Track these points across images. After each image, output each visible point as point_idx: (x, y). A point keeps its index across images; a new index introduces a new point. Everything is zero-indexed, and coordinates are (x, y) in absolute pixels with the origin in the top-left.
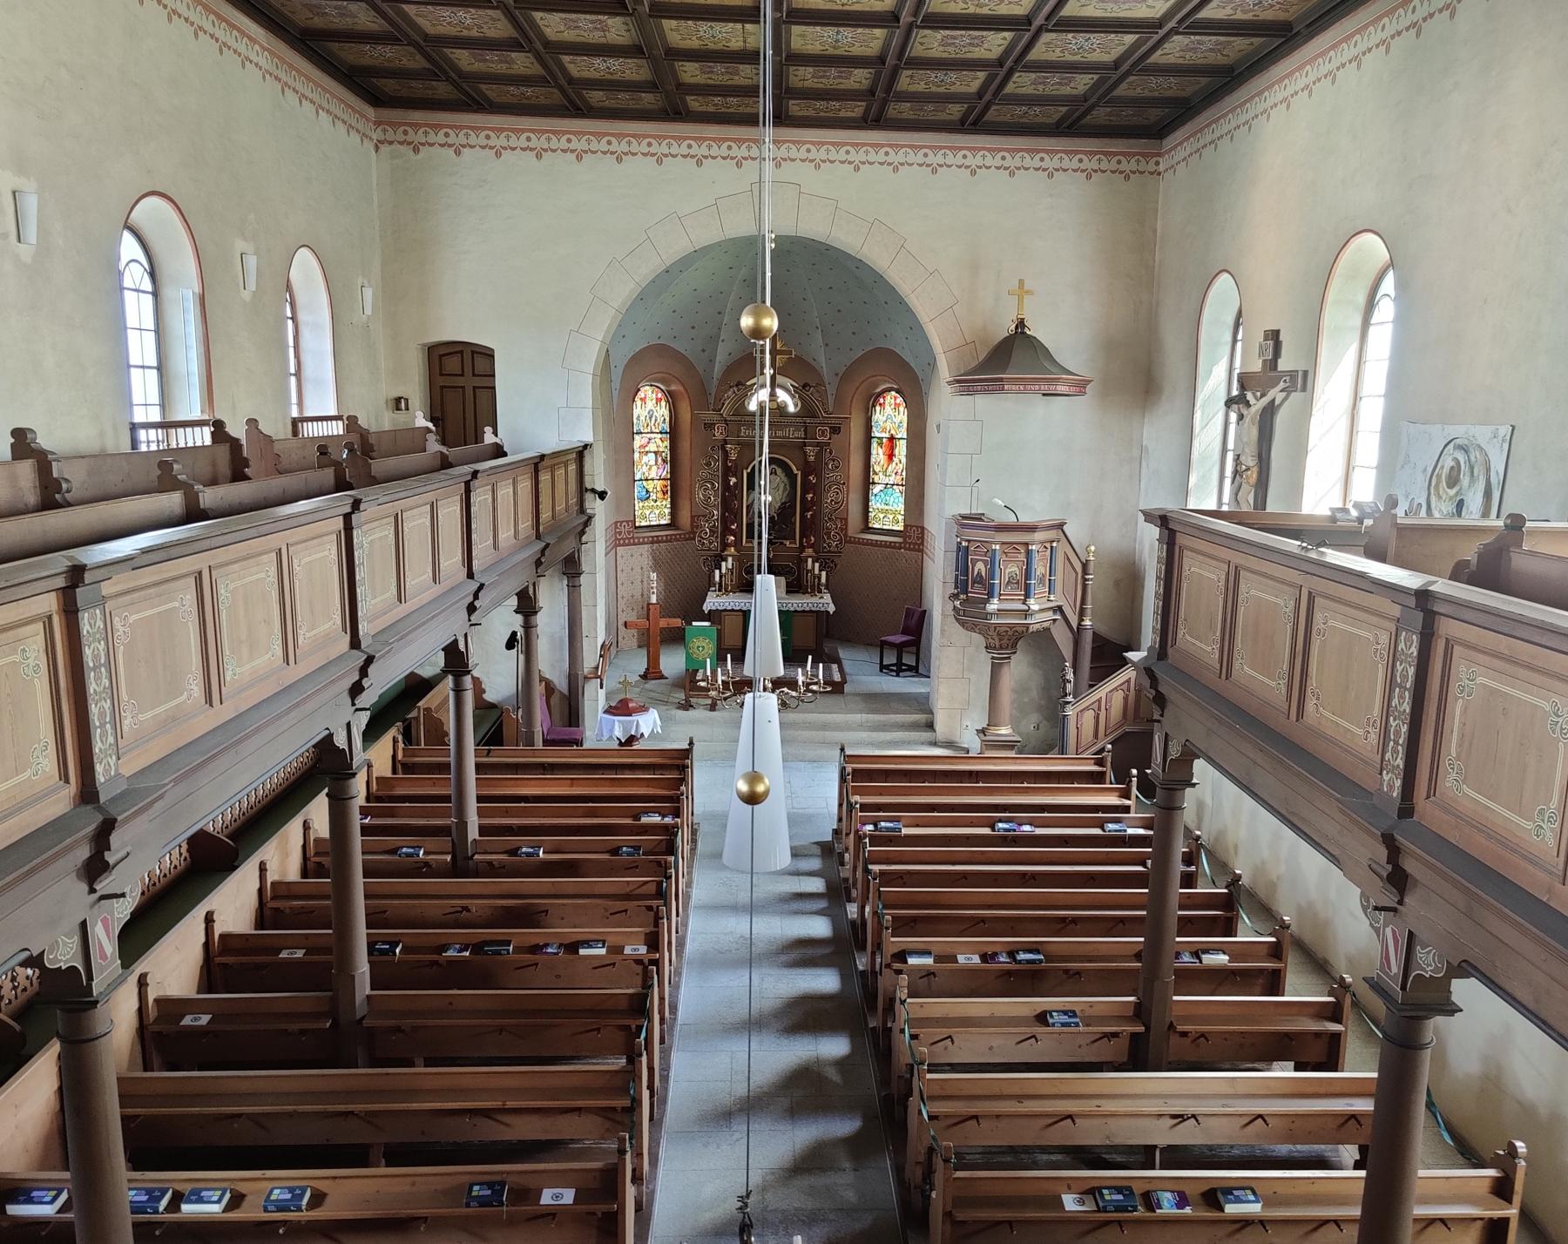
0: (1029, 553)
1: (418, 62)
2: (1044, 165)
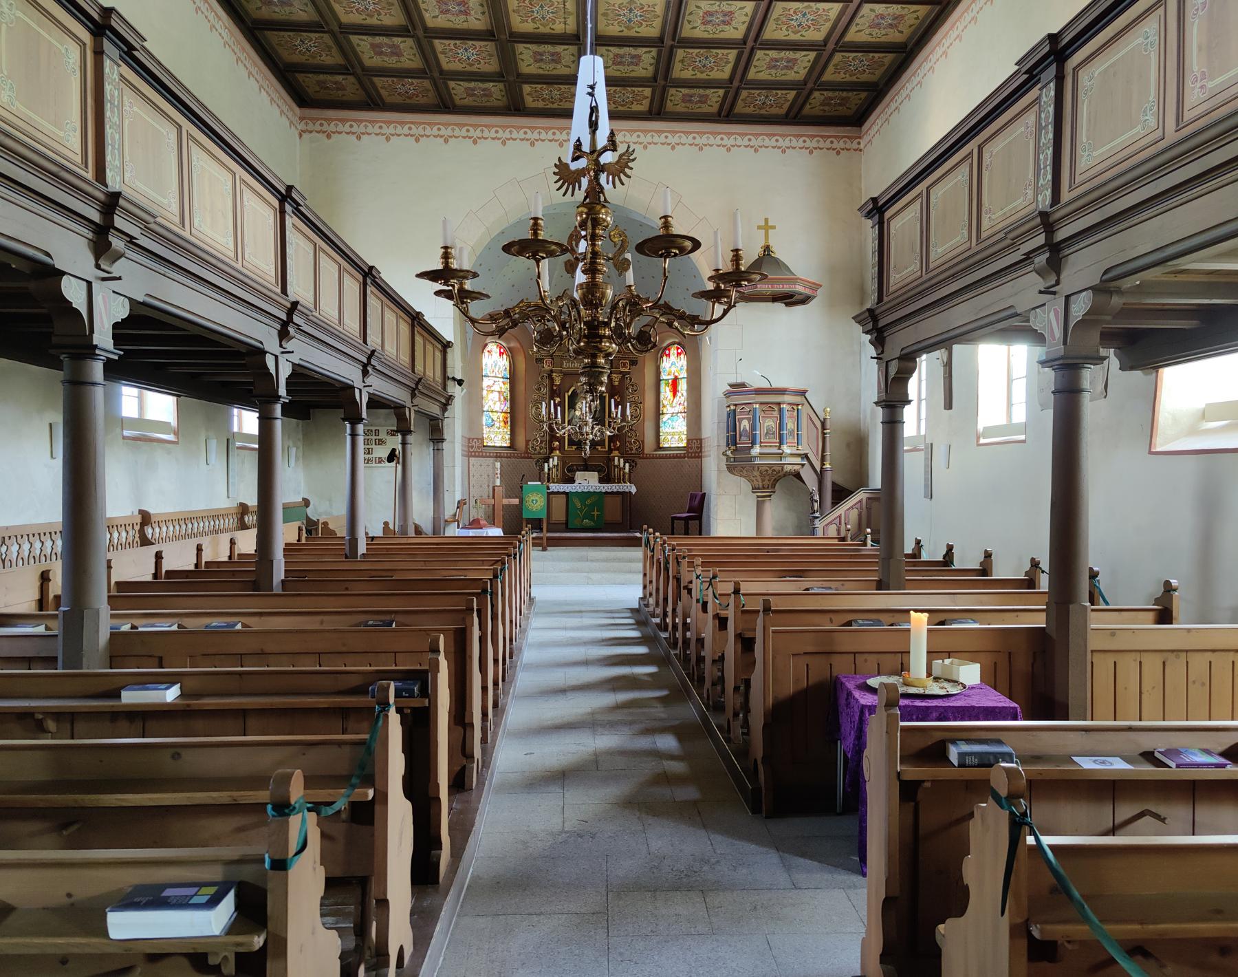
0: (780, 410)
1: (332, 58)
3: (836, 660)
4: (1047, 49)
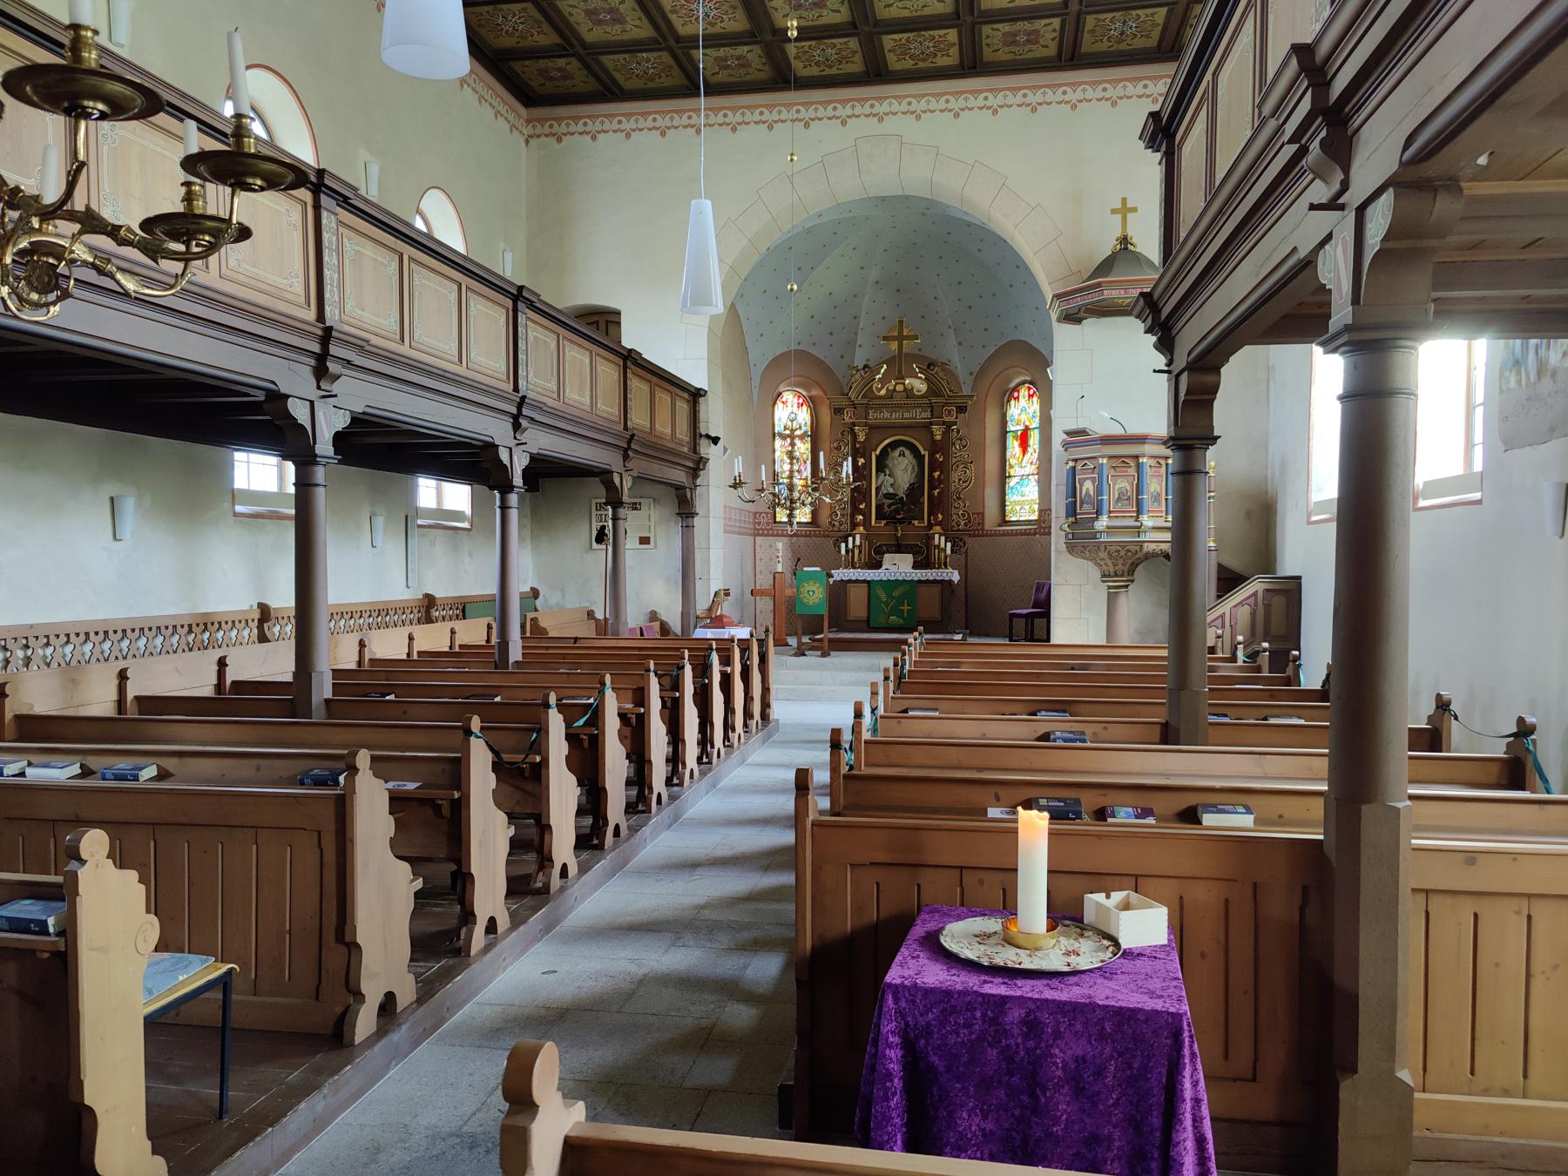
0: (1139, 466)
2: (1148, 91)
3: (927, 878)
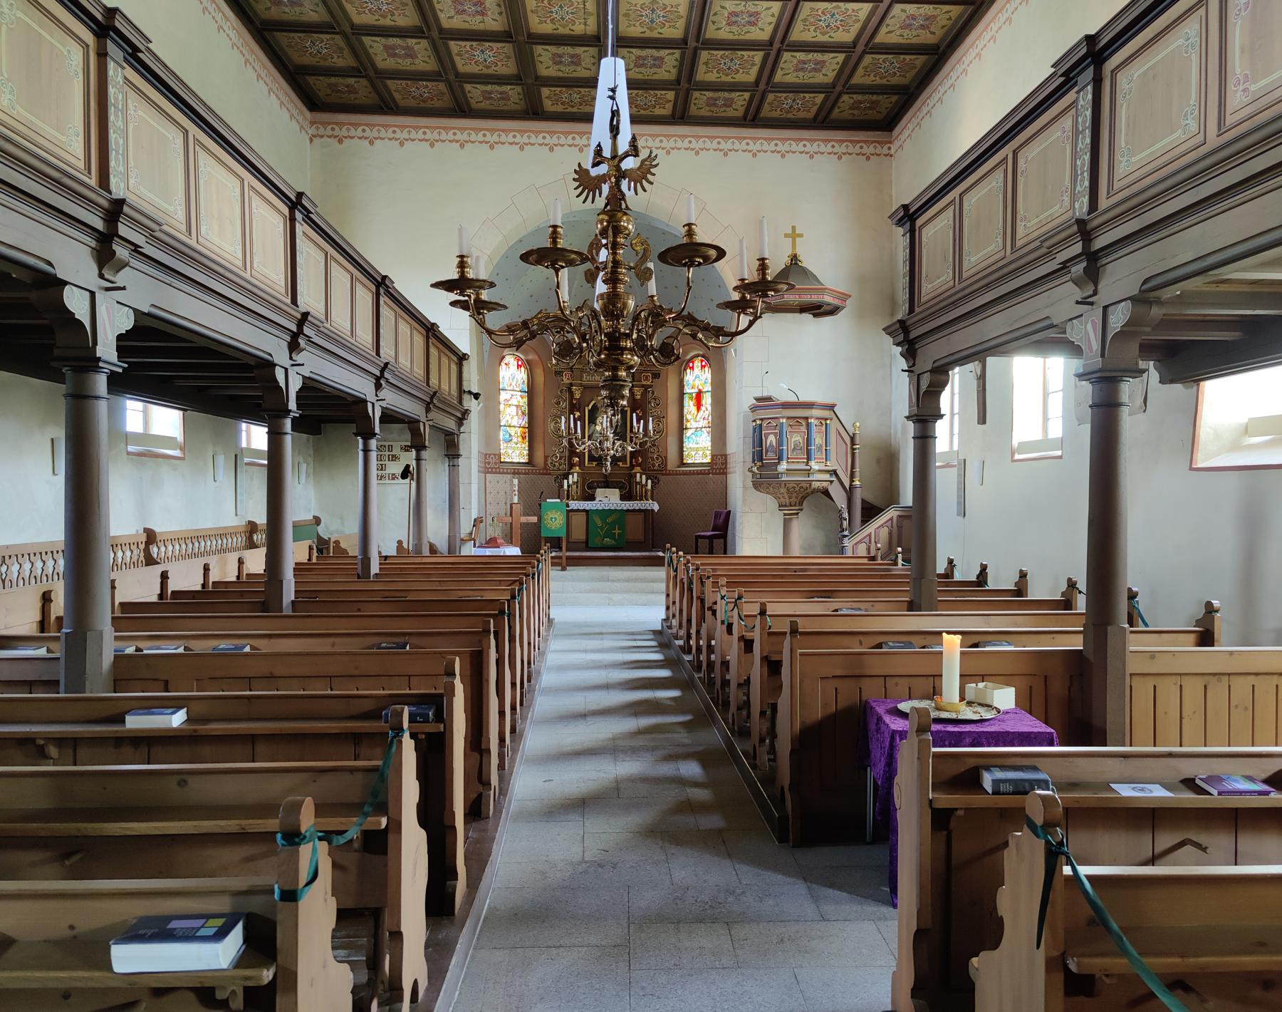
0: (808, 425)
1: (344, 60)
3: (866, 683)
4: (1084, 51)
